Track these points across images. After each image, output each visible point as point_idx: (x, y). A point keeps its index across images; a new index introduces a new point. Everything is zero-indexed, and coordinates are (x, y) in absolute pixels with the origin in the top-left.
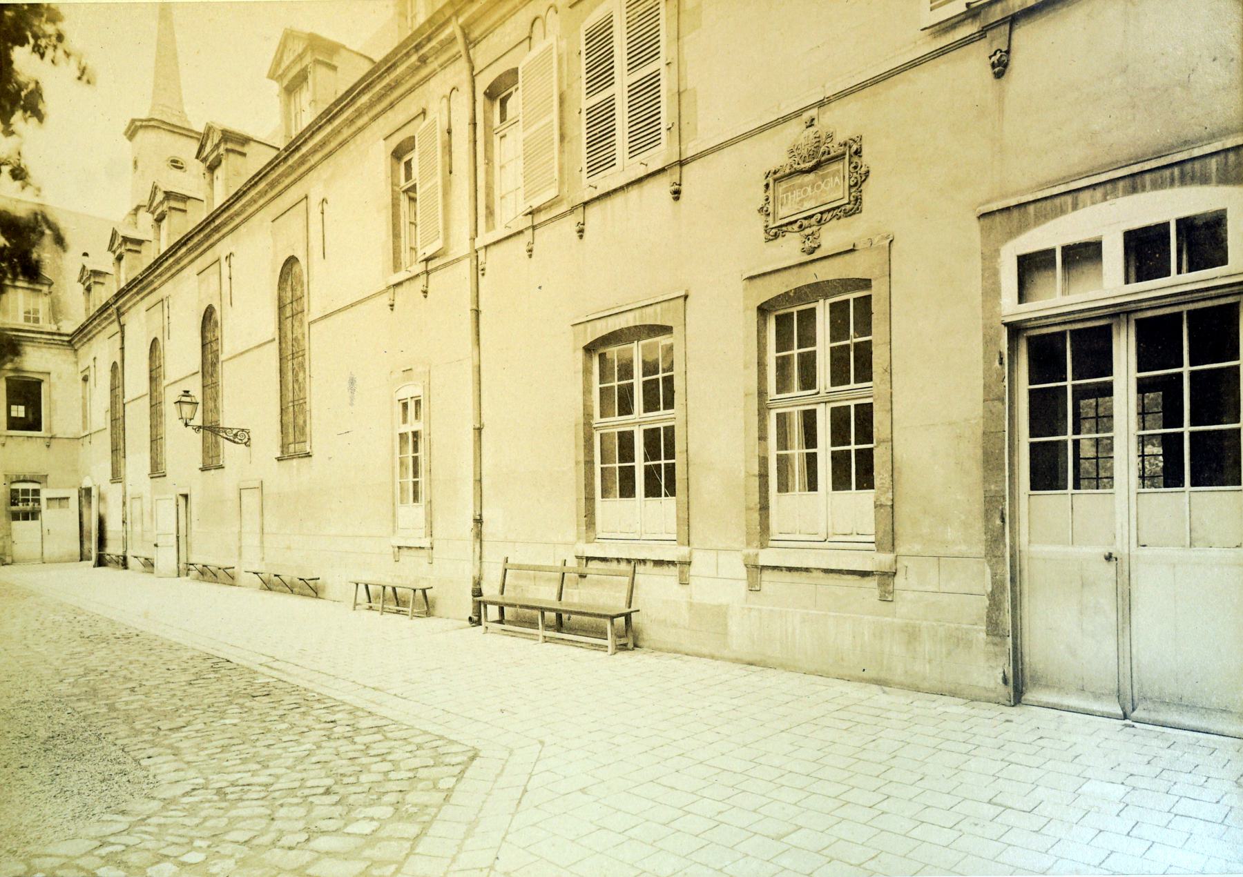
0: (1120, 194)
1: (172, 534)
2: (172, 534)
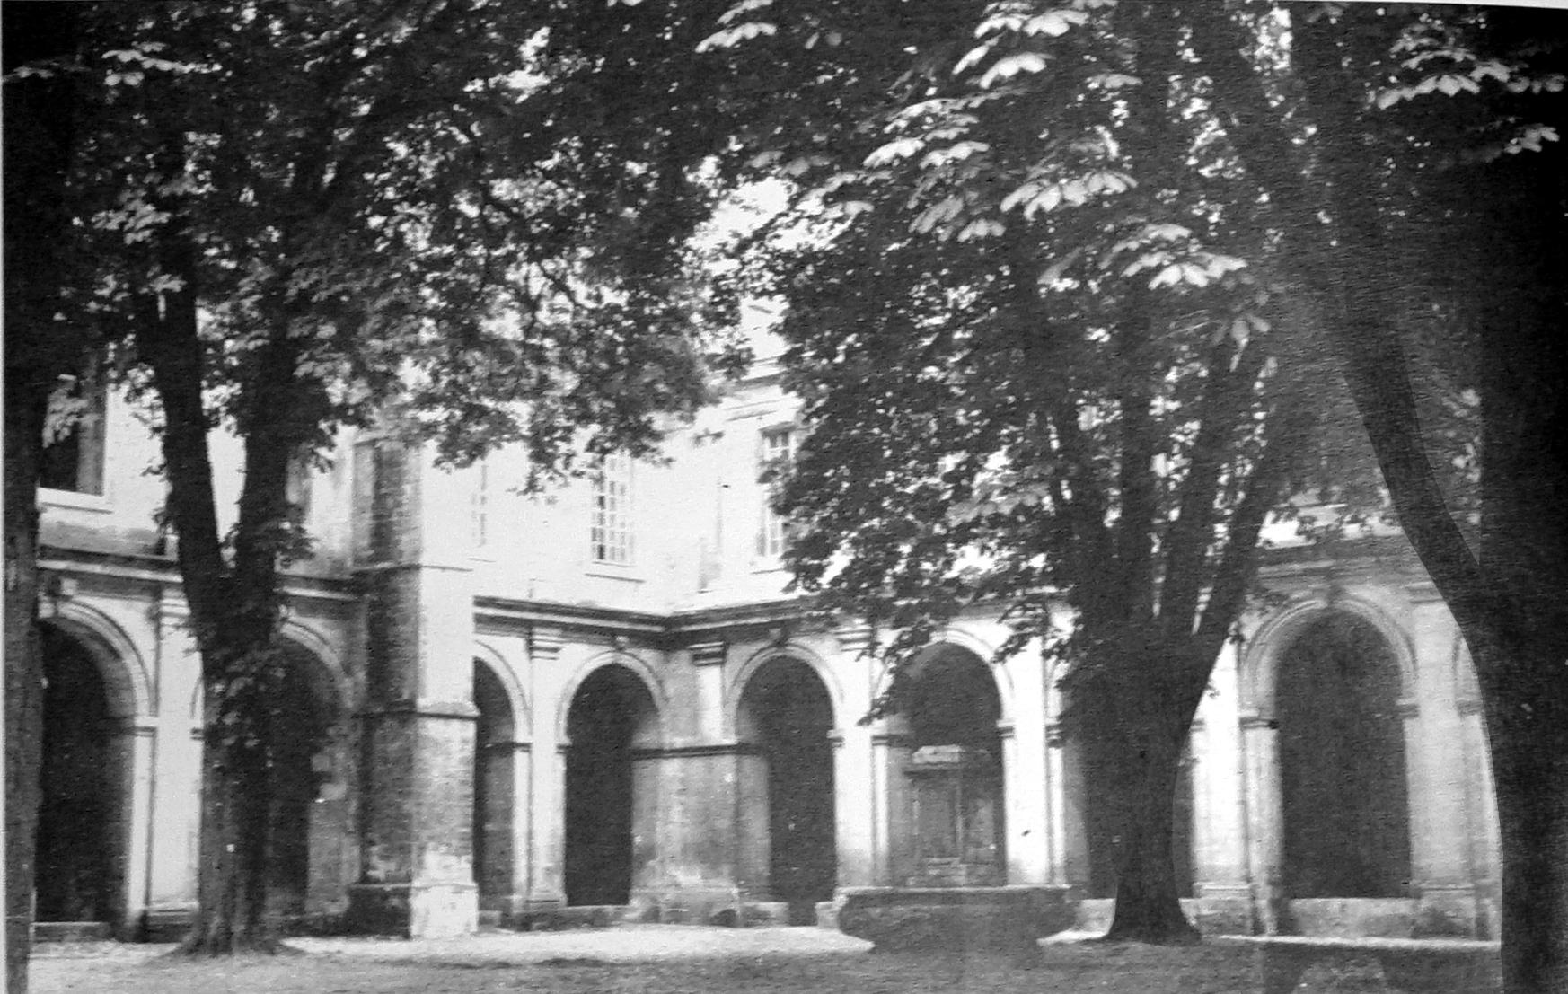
1: (1001, 657)
2: (1001, 657)
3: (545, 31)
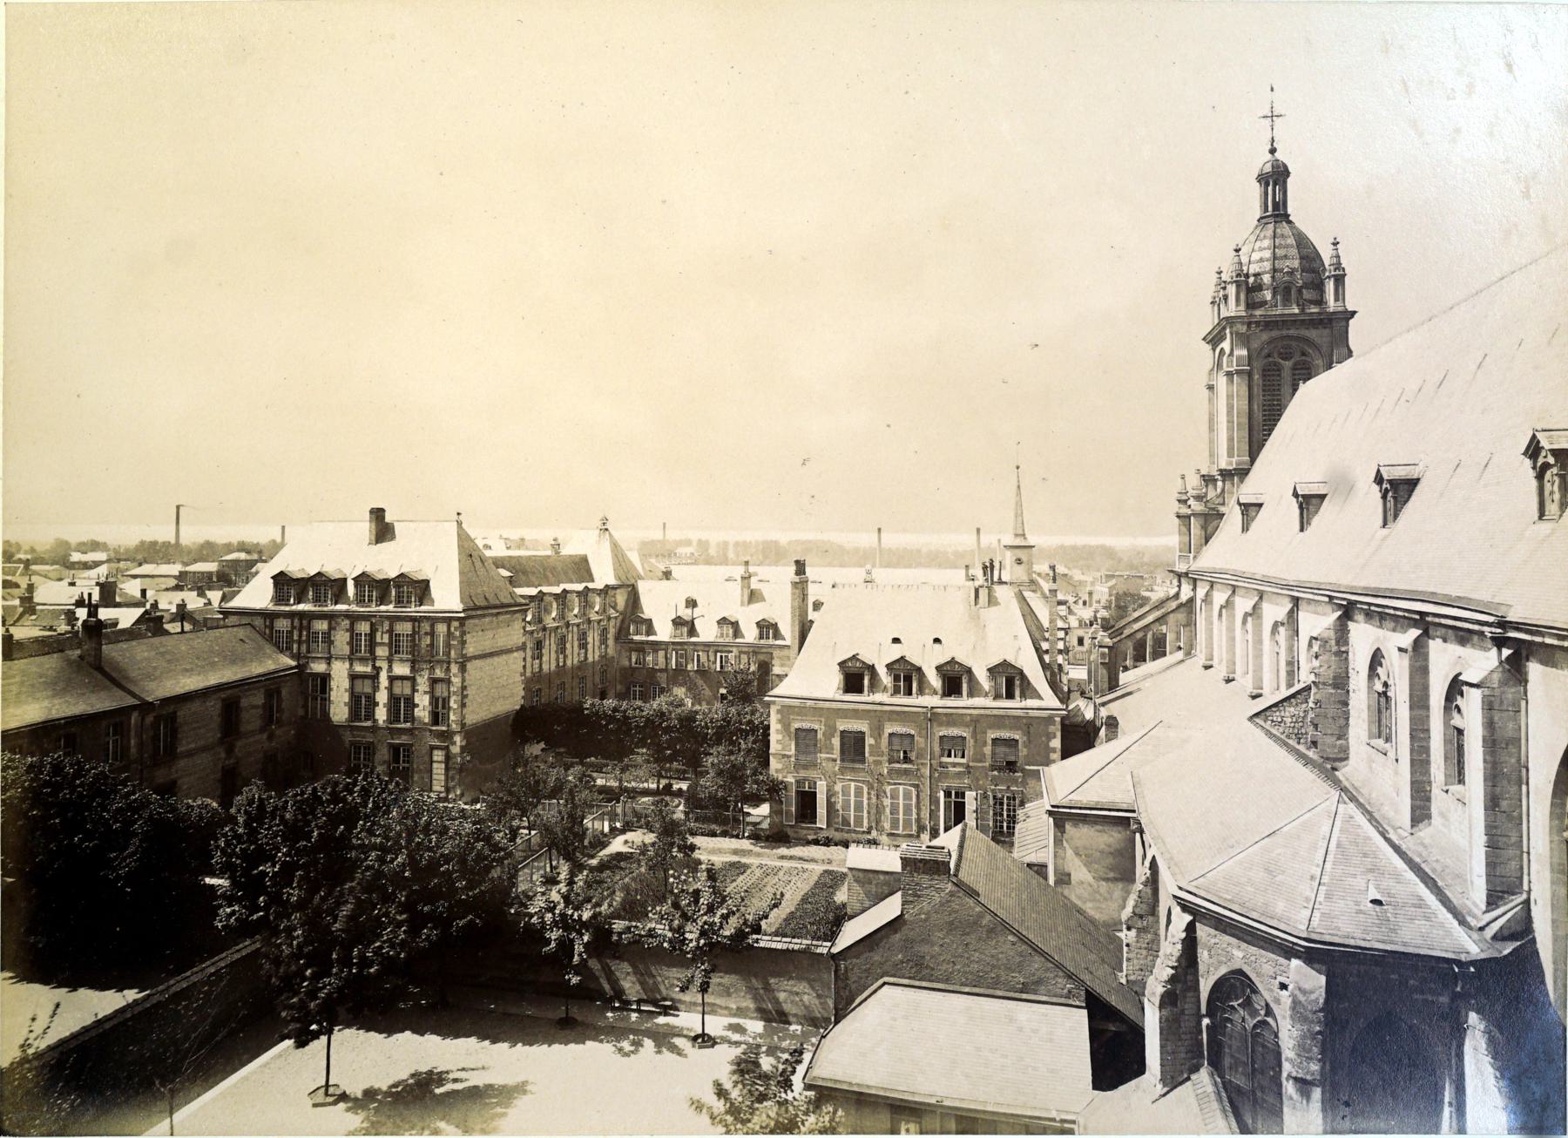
0: (1018, 698)
3: (1473, 1017)
